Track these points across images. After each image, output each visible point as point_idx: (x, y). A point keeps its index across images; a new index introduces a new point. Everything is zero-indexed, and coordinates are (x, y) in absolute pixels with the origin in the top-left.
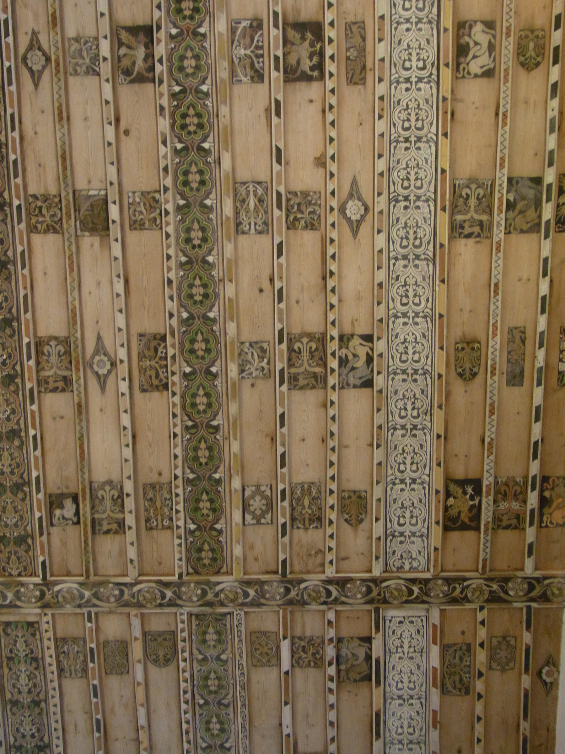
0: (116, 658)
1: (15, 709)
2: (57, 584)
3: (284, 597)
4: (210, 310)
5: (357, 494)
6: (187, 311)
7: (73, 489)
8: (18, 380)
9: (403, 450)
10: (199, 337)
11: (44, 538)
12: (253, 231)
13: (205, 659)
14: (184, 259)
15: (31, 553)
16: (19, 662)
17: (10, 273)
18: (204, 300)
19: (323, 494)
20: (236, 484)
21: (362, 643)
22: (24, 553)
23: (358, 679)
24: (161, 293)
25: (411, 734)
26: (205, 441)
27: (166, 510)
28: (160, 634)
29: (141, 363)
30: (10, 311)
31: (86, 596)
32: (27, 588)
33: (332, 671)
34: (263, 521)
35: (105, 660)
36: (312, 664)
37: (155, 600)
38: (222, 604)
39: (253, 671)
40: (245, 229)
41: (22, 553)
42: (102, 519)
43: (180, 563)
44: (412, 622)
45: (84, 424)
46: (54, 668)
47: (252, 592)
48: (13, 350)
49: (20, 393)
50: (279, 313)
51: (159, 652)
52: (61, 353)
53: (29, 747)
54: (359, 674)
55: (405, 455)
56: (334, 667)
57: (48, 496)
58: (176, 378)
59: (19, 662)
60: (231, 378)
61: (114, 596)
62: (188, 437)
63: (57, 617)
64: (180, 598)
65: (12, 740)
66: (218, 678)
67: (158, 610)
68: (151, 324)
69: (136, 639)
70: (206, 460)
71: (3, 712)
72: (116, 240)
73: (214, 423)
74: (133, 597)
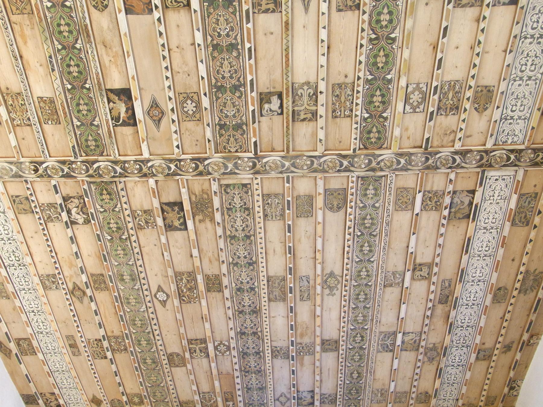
1: (233, 241)
2: (265, 158)
3: (425, 163)
5: (488, 88)
7: (279, 89)
9: (528, 54)
11: (256, 125)
13: (365, 207)
15: (245, 136)
20: (403, 82)
21: (468, 194)
22: (240, 136)
23: (461, 217)
25: (487, 251)
26: (384, 50)
27: (348, 103)
28: (336, 190)
31: (287, 166)
33: (446, 213)
34: (418, 110)
36: (434, 208)
37: (335, 167)
38: (381, 170)
39: (395, 213)
41: (238, 136)
42: (300, 111)
43: (355, 141)
44: (504, 179)
45: (290, 38)
46: (261, 214)
47: (403, 161)
49: (238, 14)
53: (243, 263)
55: (528, 58)
56: (448, 210)
59: (236, 211)
62: (371, 47)
63: (264, 180)
65: (231, 260)
66: (372, 219)
67: (337, 174)
69: (320, 194)
70: (383, 65)
71: (225, 243)
73: (393, 36)
74: (320, 166)
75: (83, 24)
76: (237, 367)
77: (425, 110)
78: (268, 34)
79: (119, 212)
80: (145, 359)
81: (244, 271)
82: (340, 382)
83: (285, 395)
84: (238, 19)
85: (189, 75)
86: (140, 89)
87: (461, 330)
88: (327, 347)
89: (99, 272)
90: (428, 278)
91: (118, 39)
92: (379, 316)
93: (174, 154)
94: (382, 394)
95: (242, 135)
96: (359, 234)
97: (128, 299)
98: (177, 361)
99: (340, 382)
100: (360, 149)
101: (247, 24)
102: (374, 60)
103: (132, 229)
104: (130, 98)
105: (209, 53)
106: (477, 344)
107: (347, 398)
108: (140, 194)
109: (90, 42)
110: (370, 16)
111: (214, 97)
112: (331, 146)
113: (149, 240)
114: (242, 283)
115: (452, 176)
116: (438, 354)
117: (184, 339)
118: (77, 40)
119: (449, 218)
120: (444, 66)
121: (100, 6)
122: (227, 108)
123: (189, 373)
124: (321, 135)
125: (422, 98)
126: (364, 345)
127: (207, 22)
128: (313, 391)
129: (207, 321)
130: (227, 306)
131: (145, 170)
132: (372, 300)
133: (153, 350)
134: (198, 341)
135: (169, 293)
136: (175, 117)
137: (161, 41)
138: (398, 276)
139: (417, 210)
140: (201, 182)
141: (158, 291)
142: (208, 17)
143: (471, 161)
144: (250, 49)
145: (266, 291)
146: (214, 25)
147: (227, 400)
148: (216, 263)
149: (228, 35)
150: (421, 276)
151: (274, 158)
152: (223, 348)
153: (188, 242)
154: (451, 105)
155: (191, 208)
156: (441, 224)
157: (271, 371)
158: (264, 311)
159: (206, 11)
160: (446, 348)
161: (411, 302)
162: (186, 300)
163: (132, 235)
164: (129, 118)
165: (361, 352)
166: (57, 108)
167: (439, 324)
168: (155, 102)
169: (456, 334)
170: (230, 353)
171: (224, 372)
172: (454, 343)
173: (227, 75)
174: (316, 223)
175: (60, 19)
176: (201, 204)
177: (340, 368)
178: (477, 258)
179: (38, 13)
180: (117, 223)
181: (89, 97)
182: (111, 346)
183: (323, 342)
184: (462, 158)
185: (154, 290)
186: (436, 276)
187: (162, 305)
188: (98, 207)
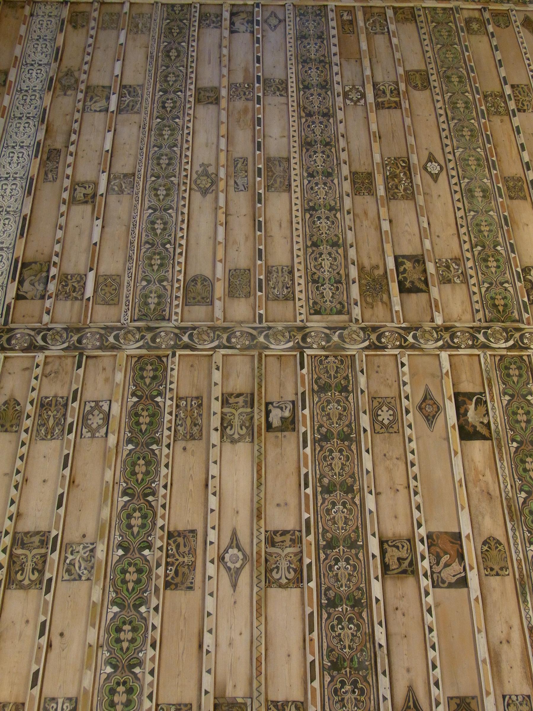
0: (239, 283)
1: (335, 239)
2: (289, 348)
4: (116, 614)
6: (140, 614)
7: (270, 435)
8: (322, 543)
10: (131, 585)
11: (300, 390)
12: (60, 701)
13: (160, 281)
14: (137, 670)
15: (315, 376)
16: (330, 279)
17: (328, 656)
18: (121, 625)
19: (35, 429)
20: (112, 439)
22: (322, 376)
23: (33, 264)
24: (165, 633)
26: (137, 481)
27: (182, 415)
28: (198, 303)
29: (193, 559)
30: (329, 615)
31: (262, 337)
33: (54, 271)
34: (93, 404)
35: (250, 281)
36: (69, 277)
37: (199, 333)
38: (138, 329)
39: (120, 272)
40: (68, 704)
42: (243, 407)
43: (173, 366)
45: (256, 499)
46: (297, 274)
47: (111, 339)
48: (326, 574)
49: (321, 530)
50: (47, 610)
51: (200, 287)
52: (276, 570)
53: (323, 210)
54: (31, 269)
56: (51, 274)
58: (159, 544)
59: (330, 279)
60: (103, 544)
61: (236, 337)
62: (153, 485)
63: (292, 318)
64: (176, 335)
65: (338, 215)
66: (151, 265)
68: (178, 598)
69: (219, 299)
70: (139, 462)
71: (346, 238)
72: (206, 692)
73: (126, 498)
74: (219, 336)
75: (516, 522)
76: (336, 69)
77: (83, 403)
78: (282, 504)
79: (483, 283)
80: (460, 82)
81: (322, 200)
82: (194, 44)
83: (271, 28)
84: (320, 524)
85: (385, 455)
86: (448, 439)
87: (29, 113)
88: (212, 94)
89: (516, 202)
90: (75, 185)
92: (141, 135)
93: (409, 355)
94: (137, 26)
95: (319, 378)
96: (168, 246)
97: (479, 165)
98: (417, 79)
99: (194, 44)
100: (167, 356)
101: (309, 518)
102: (149, 469)
103: (468, 259)
104: (461, 428)
105: (358, 483)
106: (8, 94)
107: (185, 21)
108: (455, 304)
109: (508, 500)
110: (155, 524)
111: (354, 428)
112: (205, 361)
113: (446, 243)
114: (325, 184)
115: (46, 318)
116: (60, 82)
117: (406, 108)
118: (524, 503)
119: (49, 264)
120: (60, 458)
121: (493, 544)
122: (337, 412)
123: (402, 61)
124: (217, 376)
125: (88, 419)
126: (161, 96)
127: (360, 522)
128: (232, 32)
129: (374, 133)
130: (346, 152)
131: (447, 336)
132: (151, 156)
133: (449, 94)
134: (386, 106)
135: (423, 172)
137: (418, 498)
138: (116, 189)
139: (91, 276)
141: (438, 175)
142: (357, 528)
143: (22, 337)
145: (293, 173)
146: (351, 517)
147: (351, 22)
148: (358, 211)
149: (334, 504)
150: (85, 188)
151: (279, 347)
152: (354, 96)
153: (395, 240)
154: (50, 410)
155: (388, 285)
156: (60, 255)
157: (289, 62)
158: (296, 145)
160: (49, 89)
161: (98, 153)
162: (401, 162)
163: (468, 250)
164: (464, 403)
165: (165, 85)
167: (59, 124)
168: (430, 422)
169: (36, 108)
170: (343, 88)
171: (353, 61)
172: (38, 96)
173: (336, 454)
174: (224, 261)
176: (375, 289)
177: (194, 65)
178: (11, 209)
180: (487, 267)
181: (513, 431)
182: (505, 102)
183: (217, 101)
184: (34, 341)
185: (443, 177)
186: (65, 186)
187: (433, 156)
188: (510, 289)
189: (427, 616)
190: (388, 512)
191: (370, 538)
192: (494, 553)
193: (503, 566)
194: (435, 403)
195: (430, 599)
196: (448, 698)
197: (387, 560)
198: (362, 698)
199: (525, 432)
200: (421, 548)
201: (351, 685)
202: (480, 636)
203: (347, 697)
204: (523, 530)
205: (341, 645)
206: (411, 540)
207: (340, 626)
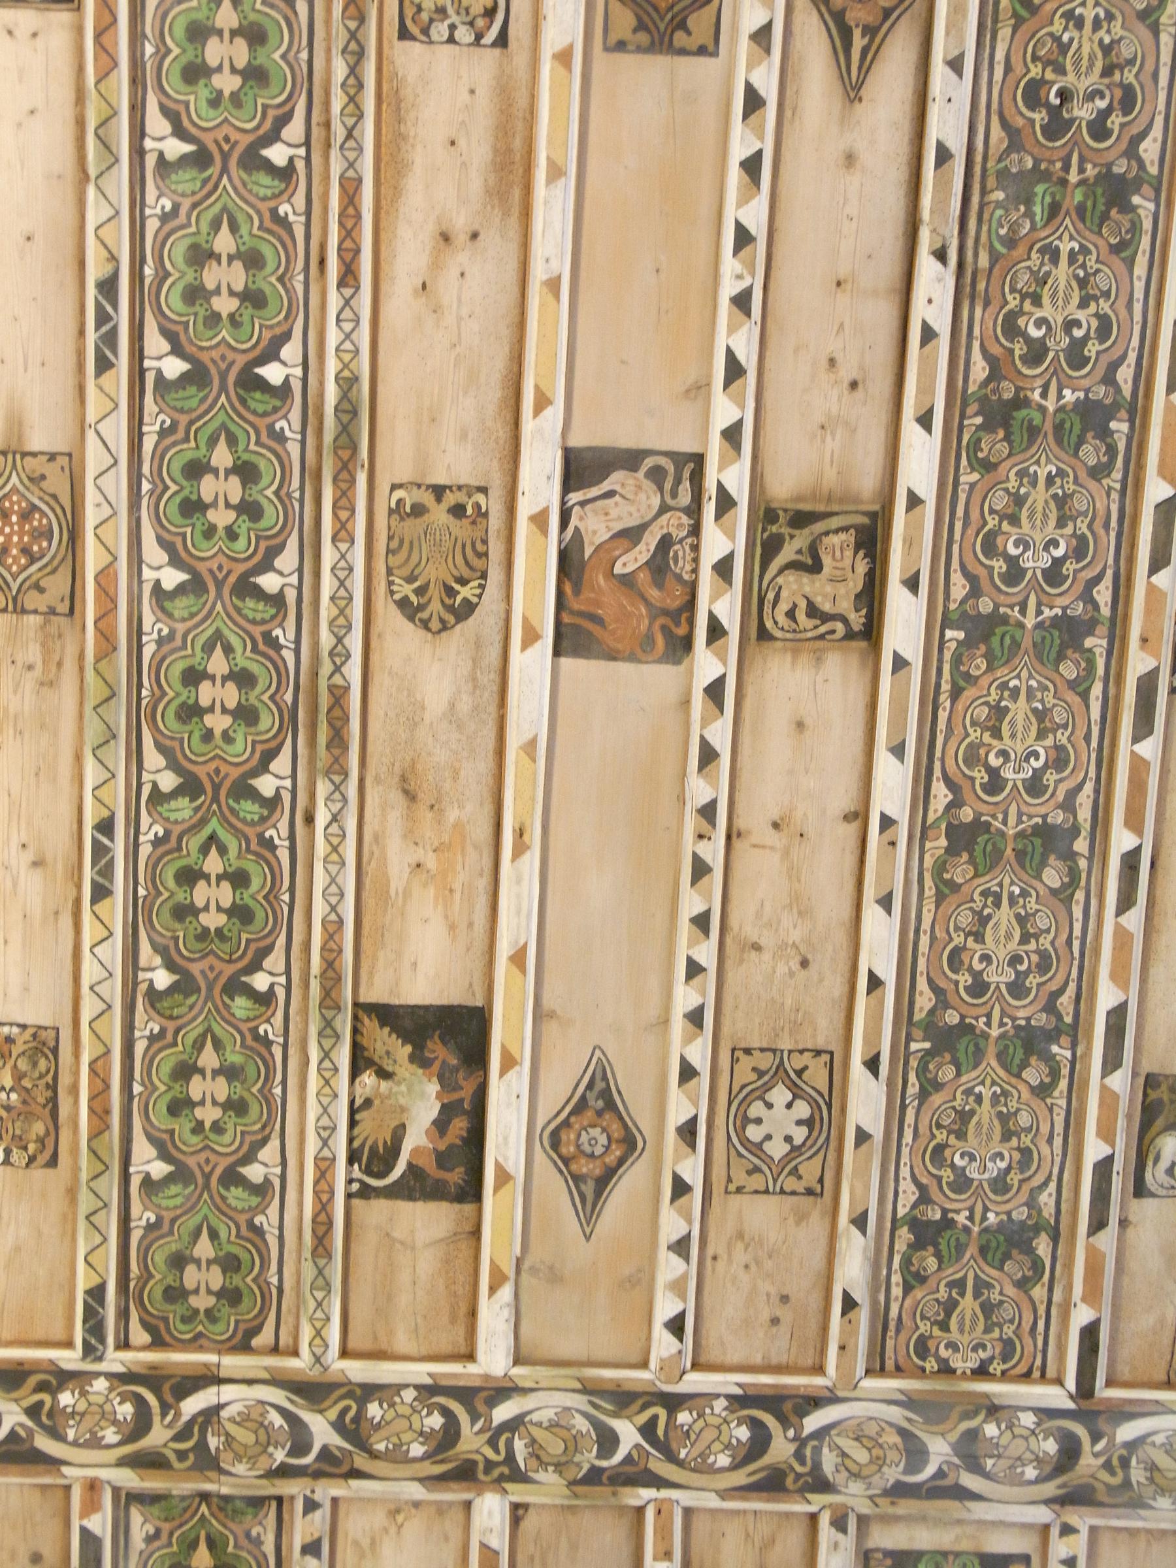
2: (1132, 1416)
8: (1096, 643)
11: (1107, 1240)
17: (1135, 228)
22: (1010, 1291)
30: (1109, 379)
32: (1010, 1427)
41: (1003, 1288)
48: (1098, 526)
49: (1097, 690)
57: (1141, 1081)
63: (1105, 1541)
84: (1095, 714)
85: (804, 963)
86: (540, 1015)
91: (484, 765)
93: (644, 1365)
95: (1023, 1284)
101: (1136, 739)
104: (475, 1055)
105: (928, 861)
109: (338, 769)
118: (270, 755)
121: (435, 607)
122: (972, 1142)
127: (943, 716)
131: (471, 1441)
136: (692, 1170)
137: (700, 790)
140: (764, 1528)
142: (956, 693)
144: (1131, 861)
146: (974, 734)
149: (1035, 786)
159: (946, 668)
164: (443, 1159)
166: (64, 1080)
168: (600, 1085)
173: (999, 977)
175: (209, 648)
179: (106, 614)
181: (256, 1037)
189: (747, 355)
190: (826, 741)
191: (914, 653)
192: (435, 572)
193: (409, 522)
194: (566, 1161)
195: (724, 411)
196: (715, 54)
197: (862, 567)
198: (1035, 71)
199: (209, 1030)
200: (726, 606)
201: (1072, 121)
202: (555, 264)
203: (1093, 80)
204: (297, 652)
205: (1083, 266)
206: (759, 633)
207: (1078, 333)
